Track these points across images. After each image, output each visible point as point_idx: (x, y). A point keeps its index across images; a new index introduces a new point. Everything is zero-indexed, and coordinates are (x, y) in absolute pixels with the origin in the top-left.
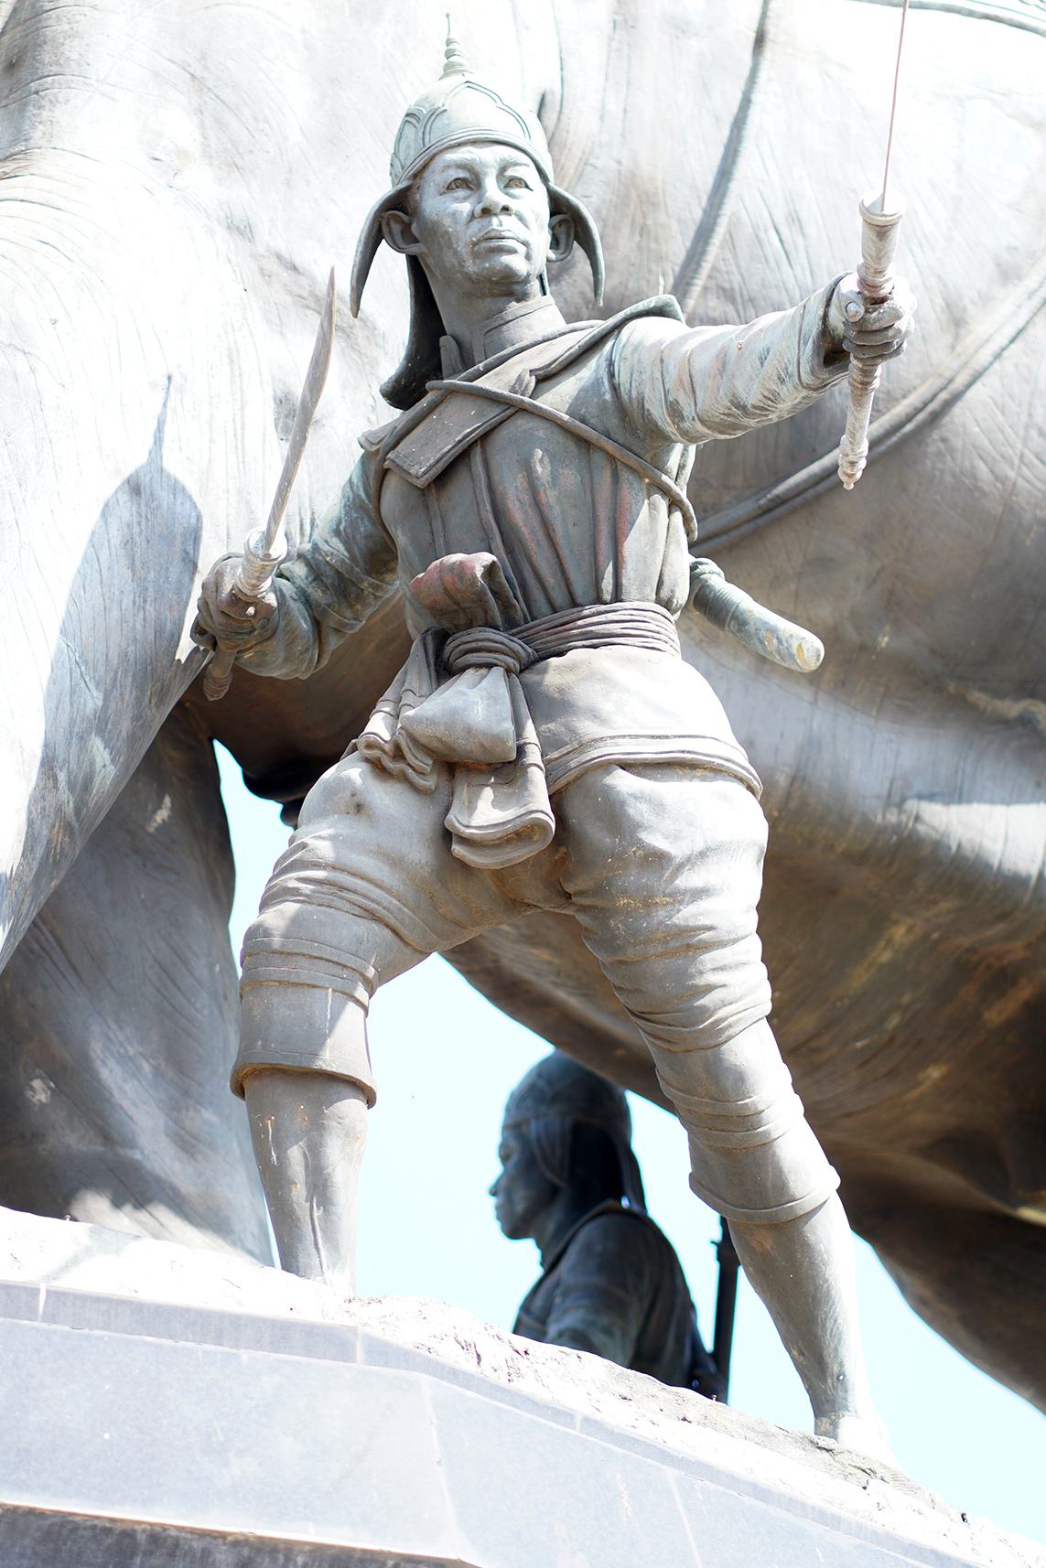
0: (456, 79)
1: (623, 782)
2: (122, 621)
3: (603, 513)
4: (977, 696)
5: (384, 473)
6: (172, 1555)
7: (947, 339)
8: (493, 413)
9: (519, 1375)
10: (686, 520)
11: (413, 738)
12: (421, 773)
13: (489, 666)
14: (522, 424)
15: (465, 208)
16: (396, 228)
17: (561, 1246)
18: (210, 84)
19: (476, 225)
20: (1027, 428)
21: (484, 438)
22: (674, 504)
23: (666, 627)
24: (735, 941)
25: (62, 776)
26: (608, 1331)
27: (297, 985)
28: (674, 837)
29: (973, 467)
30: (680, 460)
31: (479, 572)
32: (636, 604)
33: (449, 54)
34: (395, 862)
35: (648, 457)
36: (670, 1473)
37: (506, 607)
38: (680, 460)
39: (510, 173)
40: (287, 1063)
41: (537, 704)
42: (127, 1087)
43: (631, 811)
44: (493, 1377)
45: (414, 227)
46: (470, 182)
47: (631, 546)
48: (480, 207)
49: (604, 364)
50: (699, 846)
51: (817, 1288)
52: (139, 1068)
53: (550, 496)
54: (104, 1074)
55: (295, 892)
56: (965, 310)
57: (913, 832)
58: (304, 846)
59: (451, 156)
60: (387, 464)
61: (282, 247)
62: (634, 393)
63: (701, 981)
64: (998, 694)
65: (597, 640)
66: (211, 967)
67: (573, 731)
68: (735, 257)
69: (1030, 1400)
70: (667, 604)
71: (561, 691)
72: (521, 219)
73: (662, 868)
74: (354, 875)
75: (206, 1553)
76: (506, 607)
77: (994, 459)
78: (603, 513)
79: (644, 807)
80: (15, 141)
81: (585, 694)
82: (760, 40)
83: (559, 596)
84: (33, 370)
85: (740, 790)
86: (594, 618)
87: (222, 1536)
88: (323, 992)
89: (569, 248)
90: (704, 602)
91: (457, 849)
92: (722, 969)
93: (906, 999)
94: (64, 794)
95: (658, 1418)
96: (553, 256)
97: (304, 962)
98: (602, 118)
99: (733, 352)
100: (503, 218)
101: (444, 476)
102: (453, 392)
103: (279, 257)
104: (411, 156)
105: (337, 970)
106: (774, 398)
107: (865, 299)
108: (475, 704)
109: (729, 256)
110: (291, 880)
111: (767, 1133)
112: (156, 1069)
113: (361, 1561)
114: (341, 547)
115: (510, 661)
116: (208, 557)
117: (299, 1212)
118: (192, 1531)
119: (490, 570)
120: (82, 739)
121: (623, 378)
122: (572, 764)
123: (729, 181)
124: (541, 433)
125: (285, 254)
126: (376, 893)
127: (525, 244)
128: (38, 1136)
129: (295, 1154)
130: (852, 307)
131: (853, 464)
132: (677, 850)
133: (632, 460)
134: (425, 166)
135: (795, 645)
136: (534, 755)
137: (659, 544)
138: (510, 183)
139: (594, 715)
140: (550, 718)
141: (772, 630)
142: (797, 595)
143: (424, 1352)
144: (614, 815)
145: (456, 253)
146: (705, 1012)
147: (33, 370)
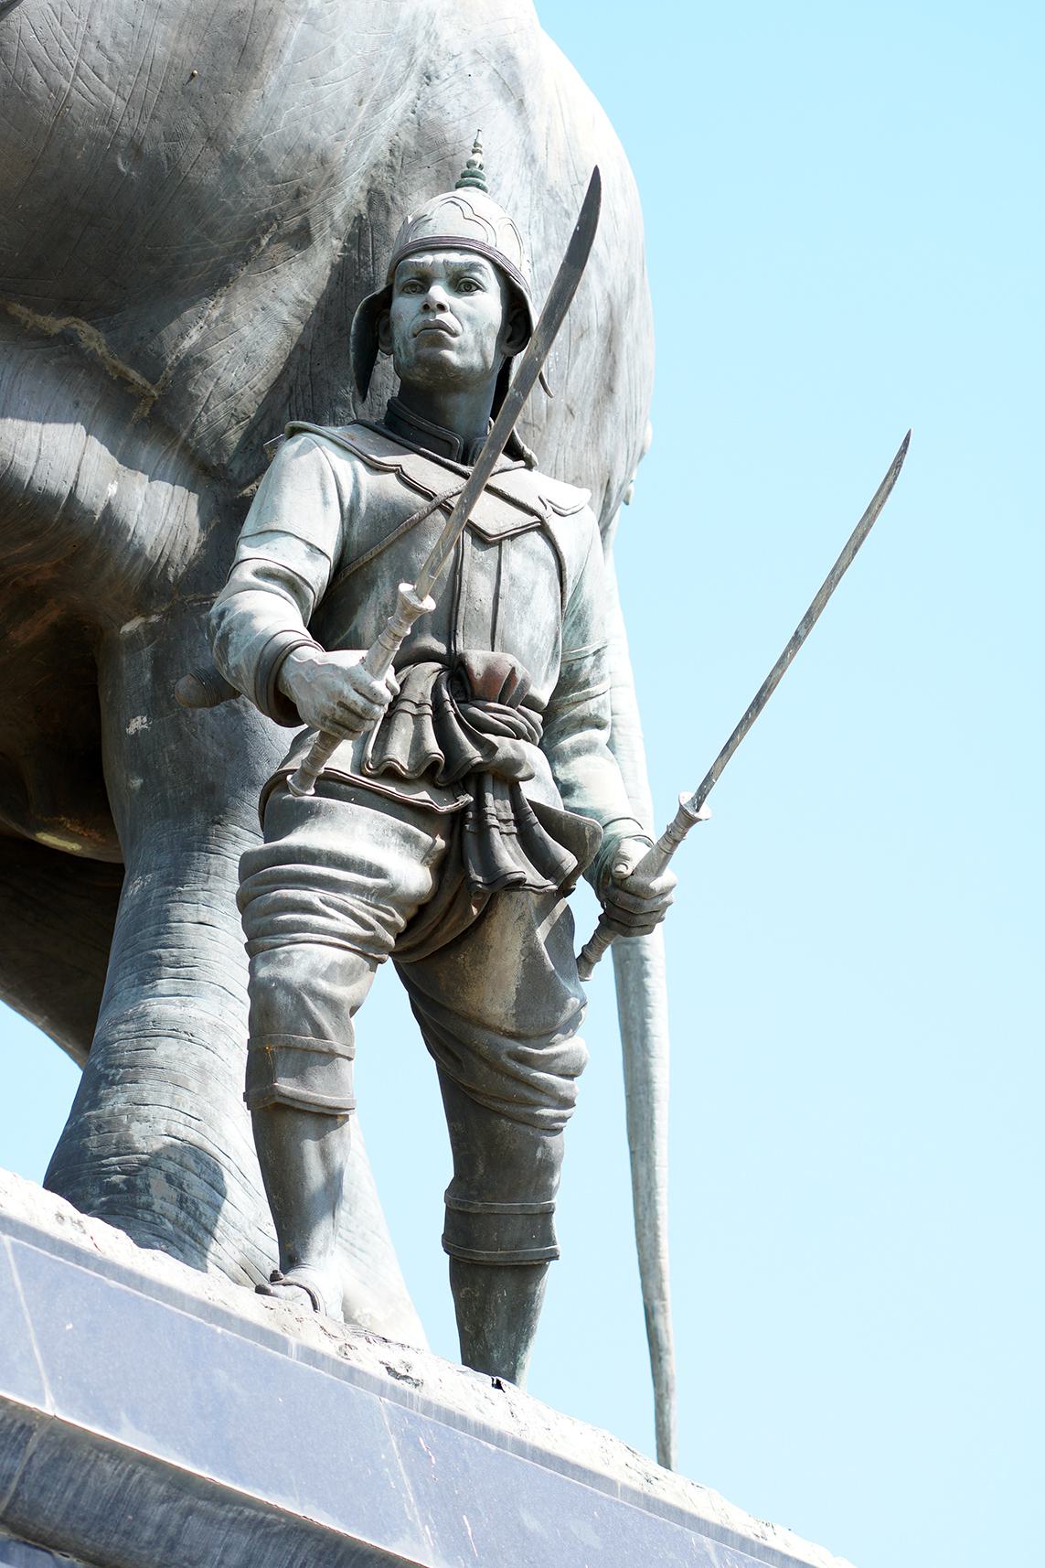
4: (17, 309)
20: (85, 39)
29: (27, 74)
64: (44, 311)
77: (49, 68)
128: (472, 368)
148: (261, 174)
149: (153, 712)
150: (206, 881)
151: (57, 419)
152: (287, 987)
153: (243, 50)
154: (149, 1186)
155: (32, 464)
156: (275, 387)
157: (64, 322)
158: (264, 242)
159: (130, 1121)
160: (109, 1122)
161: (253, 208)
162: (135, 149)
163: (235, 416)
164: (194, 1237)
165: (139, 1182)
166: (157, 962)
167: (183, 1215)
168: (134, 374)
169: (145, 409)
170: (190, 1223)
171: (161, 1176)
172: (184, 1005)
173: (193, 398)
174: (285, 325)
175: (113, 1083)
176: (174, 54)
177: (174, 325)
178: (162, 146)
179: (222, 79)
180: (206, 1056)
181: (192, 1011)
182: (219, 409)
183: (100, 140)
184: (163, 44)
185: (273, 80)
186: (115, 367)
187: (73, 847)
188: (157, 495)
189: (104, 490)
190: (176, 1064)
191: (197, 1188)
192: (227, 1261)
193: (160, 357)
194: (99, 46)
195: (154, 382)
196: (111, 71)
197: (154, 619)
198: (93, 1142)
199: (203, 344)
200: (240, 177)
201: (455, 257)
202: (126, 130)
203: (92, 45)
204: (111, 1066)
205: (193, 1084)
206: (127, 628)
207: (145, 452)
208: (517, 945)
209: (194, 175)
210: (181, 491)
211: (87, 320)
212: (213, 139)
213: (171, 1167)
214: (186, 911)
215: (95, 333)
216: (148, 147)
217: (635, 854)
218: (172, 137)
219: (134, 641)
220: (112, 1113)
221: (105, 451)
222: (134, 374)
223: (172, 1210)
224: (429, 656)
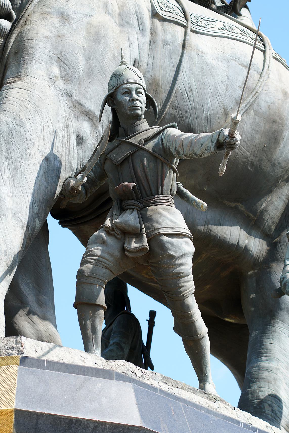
0: (124, 66)
1: (165, 239)
2: (43, 190)
3: (159, 174)
4: (225, 202)
5: (106, 159)
6: (80, 424)
7: (224, 119)
8: (134, 149)
9: (144, 378)
10: (177, 175)
11: (116, 226)
12: (118, 235)
13: (133, 209)
14: (141, 152)
15: (128, 98)
16: (110, 101)
17: (112, 321)
18: (63, 60)
19: (130, 103)
21: (132, 154)
22: (175, 171)
23: (171, 200)
24: (188, 276)
25: (30, 228)
26: (125, 343)
27: (90, 284)
28: (175, 252)
30: (176, 161)
31: (131, 187)
32: (166, 195)
33: (122, 59)
34: (112, 255)
35: (169, 161)
36: (181, 404)
37: (137, 195)
38: (176, 161)
39: (138, 90)
40: (88, 302)
41: (145, 218)
42: (27, 290)
43: (166, 246)
44: (139, 379)
45: (115, 101)
46: (129, 92)
47: (165, 182)
48: (131, 99)
49: (160, 139)
50: (181, 254)
51: (202, 355)
52: (29, 285)
53: (148, 170)
54: (22, 287)
55: (90, 262)
56: (228, 112)
57: (210, 234)
58: (91, 251)
59: (125, 86)
60: (107, 157)
61: (78, 99)
62: (168, 146)
63: (180, 285)
65: (158, 204)
66: (46, 261)
67: (153, 226)
68: (177, 99)
69: (221, 361)
70: (172, 195)
71: (150, 216)
72: (140, 102)
73: (173, 259)
74: (103, 258)
75: (88, 424)
76: (137, 195)
78: (159, 174)
79: (169, 245)
80: (18, 73)
81: (156, 217)
82: (184, 46)
83: (149, 193)
84: (25, 131)
85: (188, 240)
86: (158, 198)
87: (92, 420)
88: (95, 286)
89: (150, 107)
90: (180, 193)
91: (126, 253)
92: (185, 282)
93: (203, 271)
94: (30, 232)
95: (172, 388)
96: (146, 109)
97: (92, 279)
98: (147, 65)
99: (194, 142)
100: (137, 102)
101: (122, 163)
102: (124, 142)
103: (77, 102)
104: (114, 83)
105: (99, 280)
106: (204, 153)
107: (230, 137)
108: (130, 218)
109: (175, 98)
110: (89, 259)
111: (194, 320)
112: (33, 286)
113: (121, 426)
114: (93, 174)
115: (138, 208)
116: (64, 175)
117: (89, 336)
118: (85, 419)
119: (134, 187)
120: (34, 219)
121: (165, 142)
122: (153, 234)
123: (176, 81)
124: (145, 154)
125: (79, 101)
126: (108, 262)
127: (141, 108)
129: (89, 322)
130: (227, 139)
131: (222, 171)
132: (176, 255)
133: (166, 162)
134: (118, 88)
135: (201, 205)
136: (144, 231)
137: (172, 181)
138: (138, 93)
139: (158, 223)
140: (147, 222)
141: (195, 201)
142: (186, 178)
143: (124, 374)
144: (162, 245)
145: (125, 109)
146: (181, 292)
147: (25, 131)
148: (279, 167)
149: (256, 293)
150: (271, 333)
151: (234, 225)
153: (276, 139)
154: (264, 407)
155: (229, 237)
156: (282, 215)
157: (236, 204)
158: (279, 182)
159: (259, 392)
160: (254, 392)
161: (278, 175)
162: (252, 165)
163: (273, 223)
164: (275, 419)
165: (262, 406)
166: (261, 353)
167: (273, 414)
168: (251, 215)
169: (253, 223)
170: (274, 416)
171: (267, 405)
172: (269, 363)
173: (264, 219)
174: (284, 201)
175: (253, 382)
176: (261, 141)
177: (260, 203)
178: (258, 163)
179: (271, 146)
180: (275, 376)
181: (271, 365)
182: (270, 221)
183: (244, 163)
184: (258, 139)
185: (282, 145)
186: (246, 213)
187: (233, 321)
188: (256, 242)
189: (245, 242)
190: (268, 378)
191: (276, 407)
192: (283, 424)
193: (257, 210)
194: (244, 141)
196: (247, 147)
197: (256, 271)
198: (250, 396)
199: (266, 206)
200: (275, 168)
202: (250, 160)
203: (243, 141)
204: (253, 378)
205: (273, 382)
206: (249, 273)
207: (253, 232)
209: (265, 169)
210: (261, 240)
211: (241, 203)
212: (269, 160)
213: (269, 403)
214: (267, 340)
215: (242, 206)
216: (255, 163)
218: (260, 160)
219: (251, 276)
220: (254, 390)
221: (245, 232)
222: (251, 215)
223: (270, 413)
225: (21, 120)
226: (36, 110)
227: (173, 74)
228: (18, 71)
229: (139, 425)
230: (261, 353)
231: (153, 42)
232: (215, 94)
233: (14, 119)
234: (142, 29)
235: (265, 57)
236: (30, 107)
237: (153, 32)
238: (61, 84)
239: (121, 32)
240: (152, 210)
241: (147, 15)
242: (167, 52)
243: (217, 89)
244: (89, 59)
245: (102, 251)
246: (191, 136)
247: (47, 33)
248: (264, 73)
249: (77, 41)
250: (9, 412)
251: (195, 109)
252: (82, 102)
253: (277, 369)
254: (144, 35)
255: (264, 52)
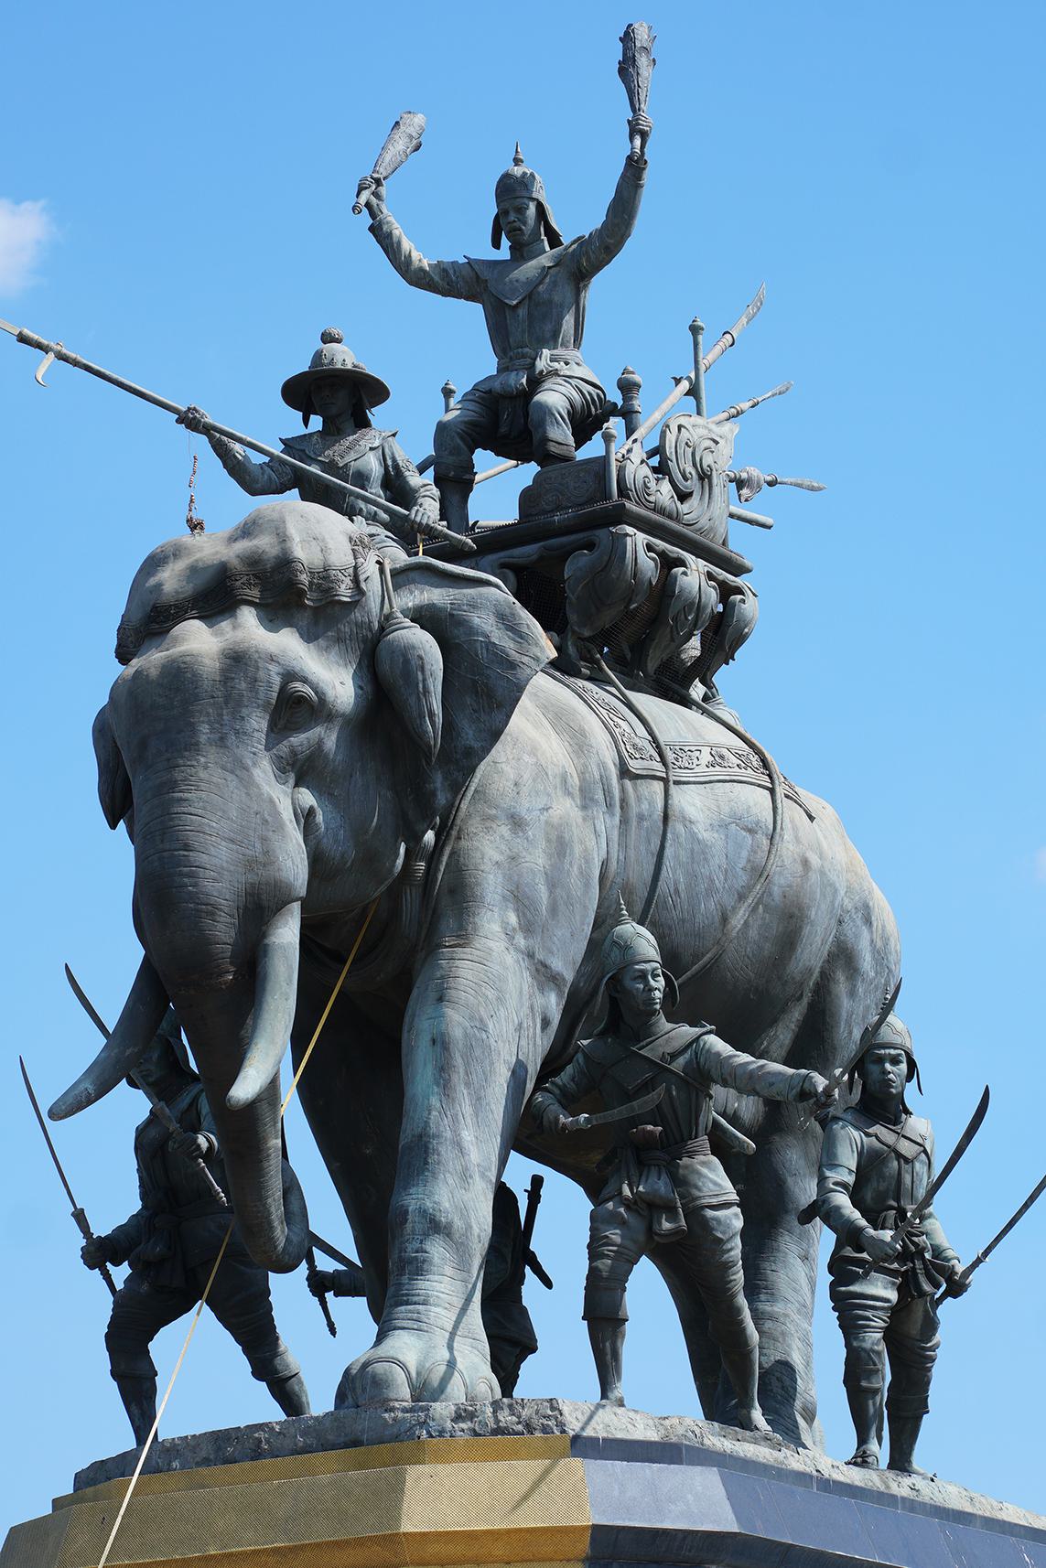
1: (710, 1213)
86: (691, 1144)
108: (658, 1185)
152: (864, 1350)
191: (788, 1382)
195: (914, 1269)
201: (893, 1052)
208: (921, 1309)
217: (960, 1268)
224: (892, 1208)
225: (481, 1020)
226: (498, 999)
227: (652, 868)
228: (461, 927)
229: (736, 1530)
230: (758, 1287)
231: (624, 821)
232: (711, 890)
233: (472, 1018)
234: (609, 806)
235: (774, 801)
236: (491, 994)
237: (624, 802)
238: (521, 941)
239: (584, 819)
240: (686, 1167)
241: (613, 772)
242: (643, 833)
243: (712, 881)
244: (552, 886)
245: (623, 1237)
246: (748, 1063)
247: (497, 857)
248: (777, 837)
249: (537, 859)
250: (584, 1528)
251: (683, 921)
252: (548, 963)
253: (786, 1315)
254: (612, 815)
255: (772, 791)
